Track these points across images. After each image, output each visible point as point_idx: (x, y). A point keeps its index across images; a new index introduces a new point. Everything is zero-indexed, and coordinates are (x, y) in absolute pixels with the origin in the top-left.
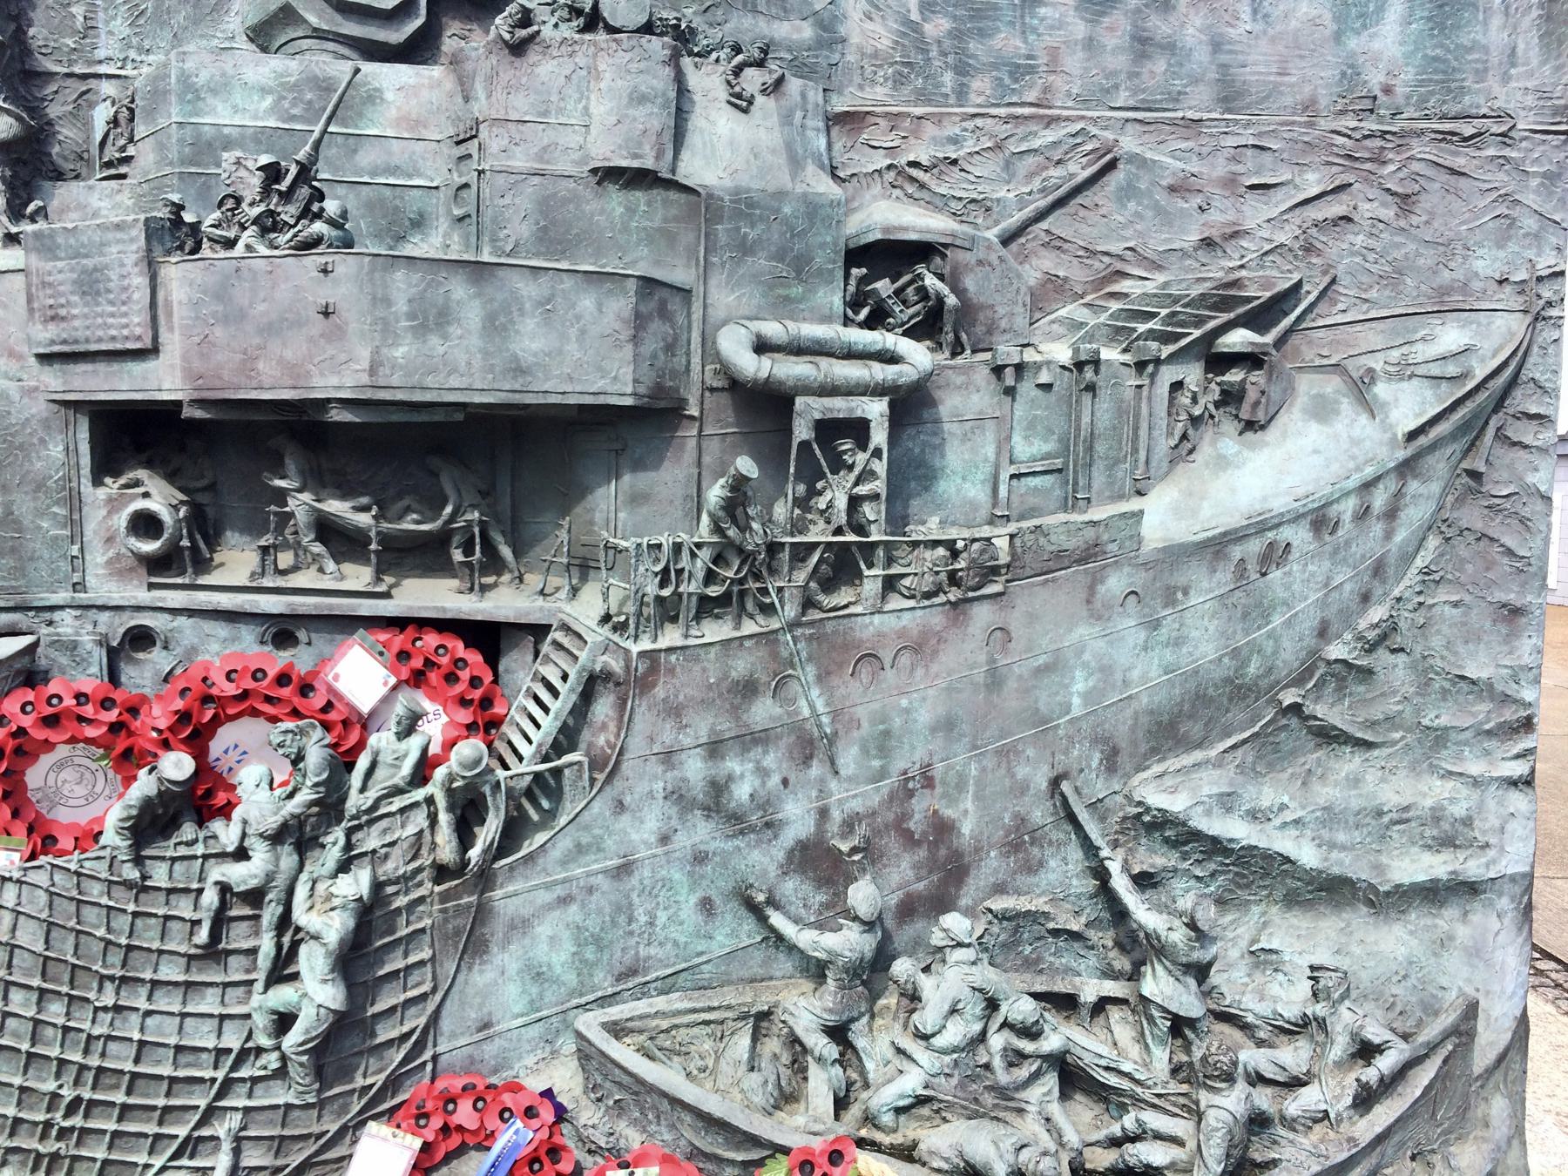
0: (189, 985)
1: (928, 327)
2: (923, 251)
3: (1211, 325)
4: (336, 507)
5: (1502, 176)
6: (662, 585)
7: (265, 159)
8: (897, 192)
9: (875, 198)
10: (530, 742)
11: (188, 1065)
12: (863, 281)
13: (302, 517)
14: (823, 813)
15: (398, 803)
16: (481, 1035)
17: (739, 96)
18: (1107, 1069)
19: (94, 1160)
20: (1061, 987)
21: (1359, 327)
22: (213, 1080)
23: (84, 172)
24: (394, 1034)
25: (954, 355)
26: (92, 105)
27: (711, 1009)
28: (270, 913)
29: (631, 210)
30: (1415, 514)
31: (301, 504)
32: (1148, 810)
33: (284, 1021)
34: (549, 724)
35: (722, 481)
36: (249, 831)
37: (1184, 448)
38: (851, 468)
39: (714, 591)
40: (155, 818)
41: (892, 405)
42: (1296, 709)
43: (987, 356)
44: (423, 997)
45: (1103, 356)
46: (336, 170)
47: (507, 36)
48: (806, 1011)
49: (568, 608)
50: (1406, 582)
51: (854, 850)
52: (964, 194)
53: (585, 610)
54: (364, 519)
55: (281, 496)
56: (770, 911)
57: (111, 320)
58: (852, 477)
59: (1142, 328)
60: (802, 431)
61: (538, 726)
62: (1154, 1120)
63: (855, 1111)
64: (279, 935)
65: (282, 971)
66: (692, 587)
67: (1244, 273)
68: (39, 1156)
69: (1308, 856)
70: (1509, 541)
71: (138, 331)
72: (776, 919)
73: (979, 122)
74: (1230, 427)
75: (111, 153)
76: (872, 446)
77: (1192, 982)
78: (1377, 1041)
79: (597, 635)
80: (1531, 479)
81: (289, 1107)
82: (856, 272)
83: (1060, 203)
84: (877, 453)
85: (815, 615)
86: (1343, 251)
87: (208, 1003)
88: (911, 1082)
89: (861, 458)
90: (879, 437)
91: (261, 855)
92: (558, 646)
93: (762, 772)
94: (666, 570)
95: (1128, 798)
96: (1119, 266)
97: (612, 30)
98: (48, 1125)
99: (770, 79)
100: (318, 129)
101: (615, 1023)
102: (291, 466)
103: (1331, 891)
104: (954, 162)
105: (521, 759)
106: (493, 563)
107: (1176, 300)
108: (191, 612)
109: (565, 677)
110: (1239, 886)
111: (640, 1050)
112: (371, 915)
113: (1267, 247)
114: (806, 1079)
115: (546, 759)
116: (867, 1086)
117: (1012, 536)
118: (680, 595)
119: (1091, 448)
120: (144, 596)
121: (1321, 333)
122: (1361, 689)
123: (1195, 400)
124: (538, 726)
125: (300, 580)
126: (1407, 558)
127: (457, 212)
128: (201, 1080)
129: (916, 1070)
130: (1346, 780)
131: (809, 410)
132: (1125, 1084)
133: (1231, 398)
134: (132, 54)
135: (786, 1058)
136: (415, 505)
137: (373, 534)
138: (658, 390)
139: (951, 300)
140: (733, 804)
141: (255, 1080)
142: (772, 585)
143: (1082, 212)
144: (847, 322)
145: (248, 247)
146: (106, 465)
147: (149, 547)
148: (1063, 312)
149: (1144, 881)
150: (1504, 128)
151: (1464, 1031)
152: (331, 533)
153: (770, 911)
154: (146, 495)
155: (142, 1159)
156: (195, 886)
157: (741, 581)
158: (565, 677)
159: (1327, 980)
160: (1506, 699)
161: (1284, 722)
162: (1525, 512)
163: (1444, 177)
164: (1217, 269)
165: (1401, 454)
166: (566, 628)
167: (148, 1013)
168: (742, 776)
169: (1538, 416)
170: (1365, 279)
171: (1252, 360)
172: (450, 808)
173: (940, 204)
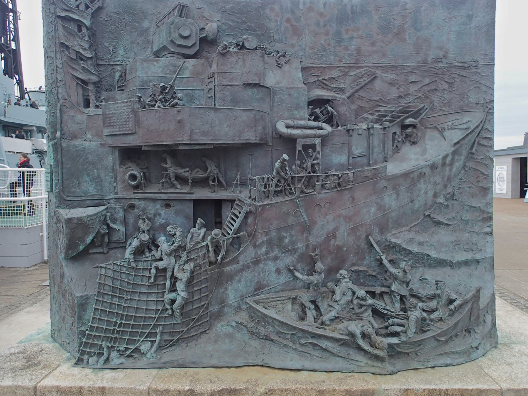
0: (149, 293)
1: (330, 120)
2: (327, 101)
3: (402, 118)
4: (181, 171)
5: (476, 77)
7: (162, 84)
8: (320, 87)
9: (314, 88)
10: (231, 230)
11: (149, 314)
12: (312, 109)
13: (171, 174)
14: (307, 246)
15: (199, 246)
16: (221, 306)
17: (279, 64)
18: (384, 309)
19: (125, 339)
21: (441, 117)
22: (155, 317)
23: (112, 89)
25: (337, 127)
26: (114, 72)
27: (280, 297)
28: (169, 274)
29: (253, 94)
30: (458, 164)
32: (391, 243)
33: (173, 301)
34: (236, 225)
35: (279, 161)
36: (163, 253)
37: (397, 150)
38: (312, 156)
39: (277, 189)
40: (139, 251)
42: (429, 215)
43: (345, 127)
45: (375, 126)
46: (178, 87)
47: (221, 52)
48: (305, 297)
49: (240, 195)
51: (316, 255)
52: (337, 86)
54: (187, 174)
55: (166, 169)
56: (295, 271)
57: (124, 126)
59: (384, 119)
60: (299, 148)
61: (233, 226)
62: (396, 320)
63: (319, 321)
64: (171, 280)
65: (173, 289)
67: (410, 104)
69: (434, 254)
71: (131, 128)
72: (297, 274)
73: (340, 68)
74: (408, 143)
75: (120, 84)
76: (317, 151)
77: (405, 286)
78: (454, 298)
80: (487, 154)
82: (311, 107)
84: (318, 153)
87: (153, 298)
88: (333, 314)
89: (314, 154)
92: (238, 205)
93: (291, 236)
94: (265, 184)
95: (386, 240)
98: (114, 330)
100: (175, 76)
101: (257, 300)
102: (168, 161)
103: (441, 263)
104: (334, 78)
105: (229, 234)
107: (393, 111)
108: (144, 199)
109: (240, 213)
110: (416, 263)
111: (264, 307)
113: (416, 97)
114: (306, 314)
116: (322, 315)
117: (353, 173)
118: (269, 191)
119: (373, 150)
120: (133, 196)
122: (446, 210)
124: (233, 226)
125: (172, 190)
127: (209, 96)
129: (335, 310)
130: (444, 236)
131: (300, 143)
132: (389, 313)
134: (125, 59)
135: (300, 309)
136: (199, 170)
137: (189, 178)
139: (335, 113)
140: (284, 244)
141: (165, 317)
143: (368, 90)
144: (309, 120)
145: (159, 107)
146: (122, 162)
148: (364, 116)
150: (476, 64)
151: (476, 297)
152: (179, 179)
153: (295, 271)
154: (132, 170)
155: (138, 338)
156: (149, 268)
158: (240, 213)
159: (440, 284)
160: (483, 211)
161: (426, 219)
162: (486, 163)
164: (403, 102)
165: (453, 149)
166: (240, 200)
167: (139, 300)
168: (286, 237)
169: (489, 138)
170: (441, 104)
171: (414, 126)
172: (212, 247)
173: (331, 89)
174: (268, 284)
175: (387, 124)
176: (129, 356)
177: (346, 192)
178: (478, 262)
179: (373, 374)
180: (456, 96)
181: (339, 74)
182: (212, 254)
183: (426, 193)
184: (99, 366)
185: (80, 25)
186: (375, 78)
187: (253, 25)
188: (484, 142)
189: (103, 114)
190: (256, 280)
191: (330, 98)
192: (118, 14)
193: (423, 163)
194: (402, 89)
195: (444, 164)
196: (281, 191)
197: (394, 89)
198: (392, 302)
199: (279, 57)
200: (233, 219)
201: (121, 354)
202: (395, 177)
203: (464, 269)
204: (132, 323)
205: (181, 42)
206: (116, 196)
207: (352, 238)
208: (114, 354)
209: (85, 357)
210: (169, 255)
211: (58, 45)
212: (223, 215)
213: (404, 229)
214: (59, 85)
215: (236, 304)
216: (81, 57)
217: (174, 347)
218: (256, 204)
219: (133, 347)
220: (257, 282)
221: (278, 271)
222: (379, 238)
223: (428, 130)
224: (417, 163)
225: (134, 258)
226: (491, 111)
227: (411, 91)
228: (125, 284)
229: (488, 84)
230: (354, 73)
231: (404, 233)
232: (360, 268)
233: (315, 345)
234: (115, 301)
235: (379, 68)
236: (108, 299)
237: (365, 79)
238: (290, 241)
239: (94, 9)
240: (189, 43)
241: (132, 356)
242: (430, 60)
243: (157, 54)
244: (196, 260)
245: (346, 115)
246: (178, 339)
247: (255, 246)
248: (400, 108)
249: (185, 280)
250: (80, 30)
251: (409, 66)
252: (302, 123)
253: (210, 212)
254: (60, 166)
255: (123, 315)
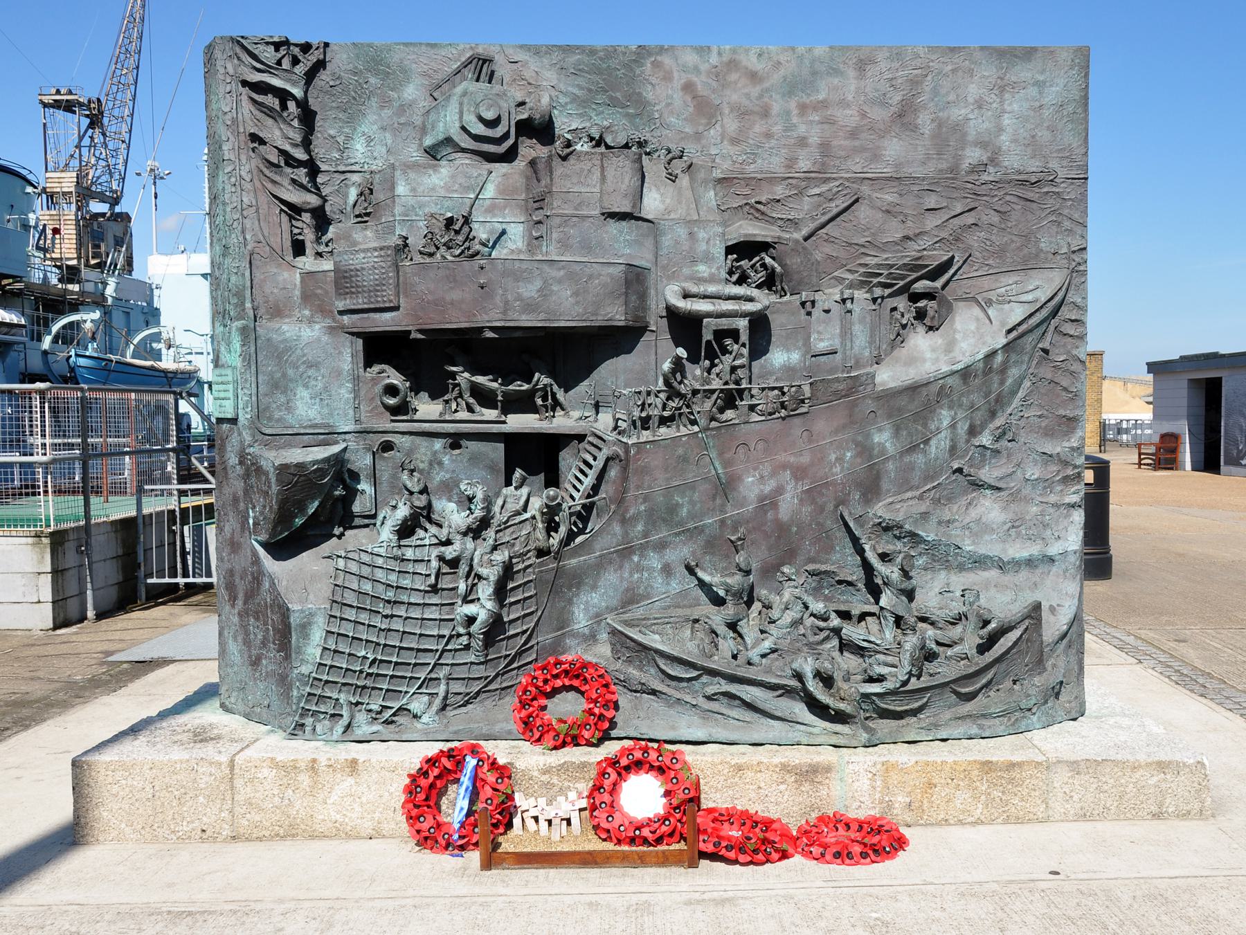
0: (425, 604)
1: (770, 282)
2: (764, 247)
3: (909, 279)
4: (480, 379)
6: (642, 410)
12: (737, 260)
15: (519, 519)
20: (842, 608)
24: (519, 630)
31: (464, 378)
37: (899, 339)
39: (666, 414)
41: (750, 321)
42: (960, 470)
44: (532, 613)
49: (595, 425)
50: (1014, 406)
53: (604, 421)
54: (495, 385)
55: (453, 375)
58: (732, 357)
59: (875, 280)
60: (707, 336)
62: (881, 657)
66: (655, 412)
68: (357, 687)
69: (968, 547)
70: (1064, 384)
74: (921, 329)
79: (612, 437)
80: (1075, 352)
81: (472, 663)
83: (134, 730)
85: (714, 424)
86: (974, 240)
88: (767, 645)
90: (744, 338)
91: (457, 539)
94: (643, 404)
96: (863, 250)
97: (608, 147)
98: (361, 672)
99: (685, 166)
103: (980, 562)
104: (778, 201)
106: (557, 404)
107: (891, 266)
108: (411, 433)
112: (508, 571)
115: (589, 496)
121: (965, 282)
123: (903, 316)
126: (1014, 393)
128: (431, 651)
130: (989, 509)
133: (921, 315)
138: (637, 318)
139: (778, 269)
141: (456, 650)
142: (696, 408)
147: (392, 401)
149: (884, 557)
155: (404, 689)
157: (680, 408)
158: (595, 459)
160: (1066, 463)
163: (1022, 203)
164: (913, 250)
165: (1004, 341)
171: (930, 296)
173: (773, 221)
174: (648, 594)
175: (878, 292)
176: (388, 722)
177: (796, 421)
178: (1052, 560)
179: (835, 746)
180: (1015, 238)
181: (788, 193)
182: (540, 534)
183: (953, 426)
184: (335, 737)
185: (284, 96)
186: (857, 201)
187: (618, 95)
188: (1069, 329)
189: (337, 270)
190: (625, 584)
191: (769, 240)
192: (355, 74)
193: (945, 369)
194: (909, 224)
195: (988, 371)
196: (671, 419)
197: (894, 223)
198: (881, 630)
199: (671, 160)
200: (582, 472)
201: (375, 716)
202: (889, 396)
203: (1024, 574)
204: (394, 659)
205: (479, 129)
206: (358, 427)
207: (807, 509)
208: (361, 717)
209: (309, 721)
210: (465, 534)
211: (242, 138)
212: (563, 465)
213: (909, 494)
214: (245, 213)
215: (586, 631)
216: (290, 161)
217: (470, 706)
218: (624, 440)
219: (396, 705)
220: (627, 590)
221: (667, 570)
222: (859, 511)
223: (961, 304)
224: (934, 368)
225: (399, 539)
226: (1081, 268)
227: (928, 228)
228: (381, 588)
229: (1076, 216)
230: (817, 191)
231: (910, 503)
232: (823, 568)
233: (731, 696)
234: (364, 617)
235: (866, 182)
236: (350, 614)
237: (838, 202)
238: (689, 512)
239: (309, 64)
240: (498, 132)
241: (393, 722)
242: (965, 166)
243: (432, 153)
244: (513, 545)
245: (799, 272)
246: (478, 693)
247: (623, 521)
248: (906, 261)
249: (493, 578)
250: (284, 107)
251: (924, 179)
252: (712, 289)
253: (536, 457)
254: (253, 367)
255: (378, 644)
